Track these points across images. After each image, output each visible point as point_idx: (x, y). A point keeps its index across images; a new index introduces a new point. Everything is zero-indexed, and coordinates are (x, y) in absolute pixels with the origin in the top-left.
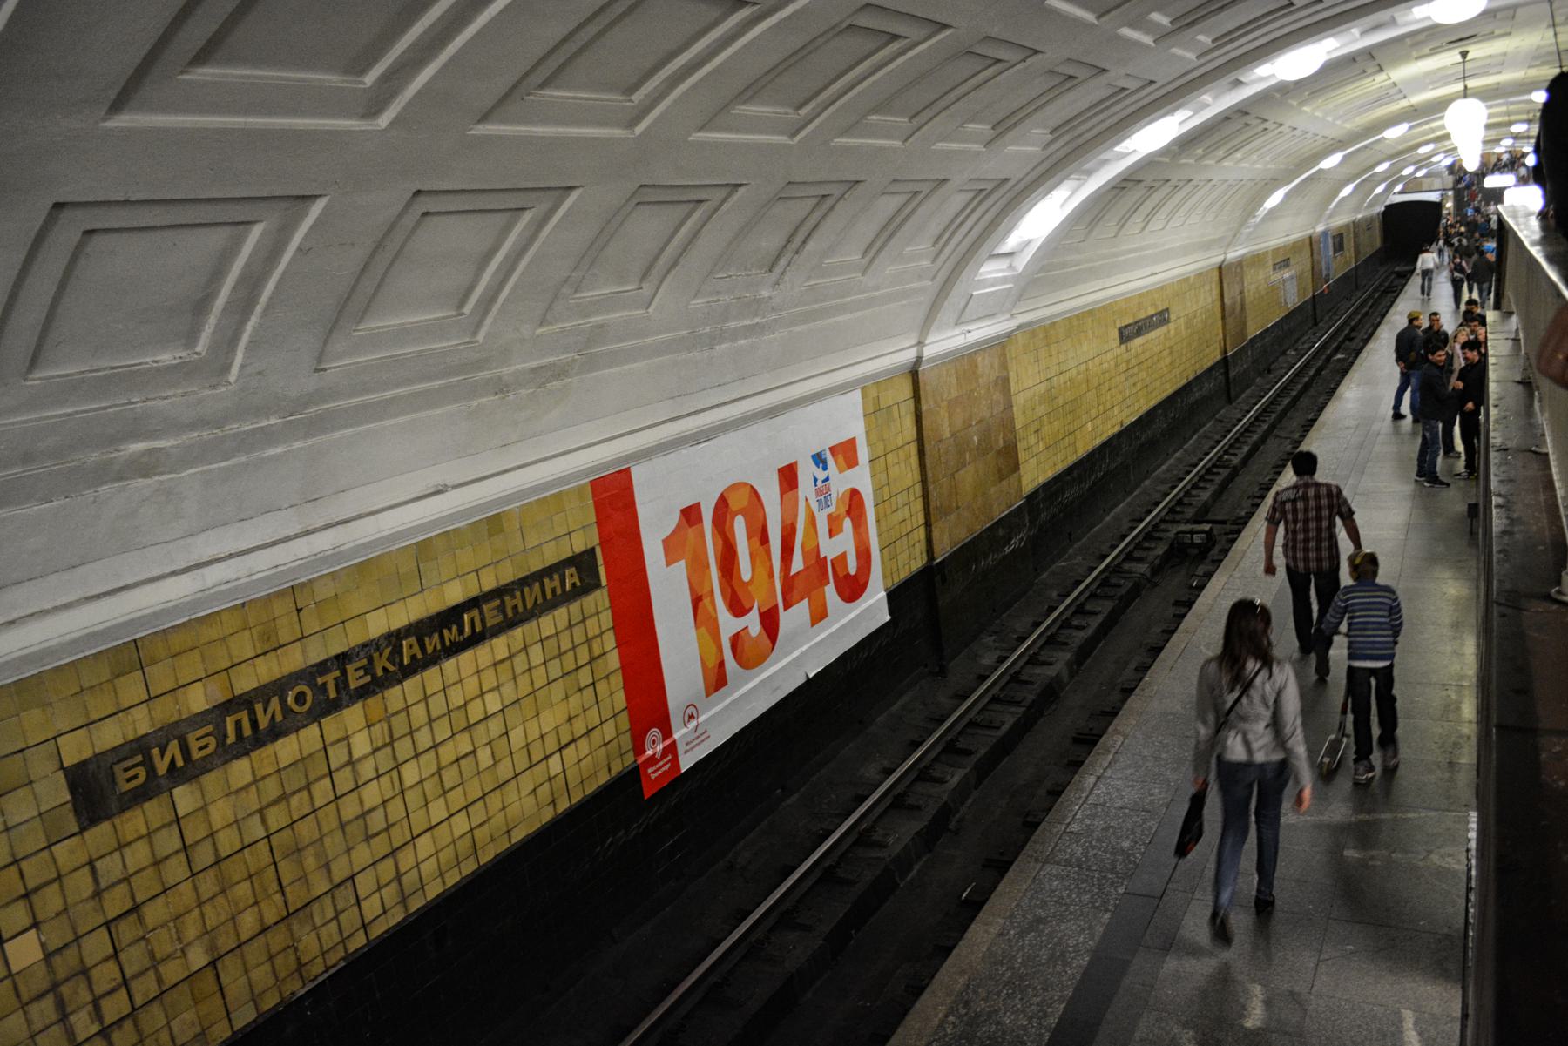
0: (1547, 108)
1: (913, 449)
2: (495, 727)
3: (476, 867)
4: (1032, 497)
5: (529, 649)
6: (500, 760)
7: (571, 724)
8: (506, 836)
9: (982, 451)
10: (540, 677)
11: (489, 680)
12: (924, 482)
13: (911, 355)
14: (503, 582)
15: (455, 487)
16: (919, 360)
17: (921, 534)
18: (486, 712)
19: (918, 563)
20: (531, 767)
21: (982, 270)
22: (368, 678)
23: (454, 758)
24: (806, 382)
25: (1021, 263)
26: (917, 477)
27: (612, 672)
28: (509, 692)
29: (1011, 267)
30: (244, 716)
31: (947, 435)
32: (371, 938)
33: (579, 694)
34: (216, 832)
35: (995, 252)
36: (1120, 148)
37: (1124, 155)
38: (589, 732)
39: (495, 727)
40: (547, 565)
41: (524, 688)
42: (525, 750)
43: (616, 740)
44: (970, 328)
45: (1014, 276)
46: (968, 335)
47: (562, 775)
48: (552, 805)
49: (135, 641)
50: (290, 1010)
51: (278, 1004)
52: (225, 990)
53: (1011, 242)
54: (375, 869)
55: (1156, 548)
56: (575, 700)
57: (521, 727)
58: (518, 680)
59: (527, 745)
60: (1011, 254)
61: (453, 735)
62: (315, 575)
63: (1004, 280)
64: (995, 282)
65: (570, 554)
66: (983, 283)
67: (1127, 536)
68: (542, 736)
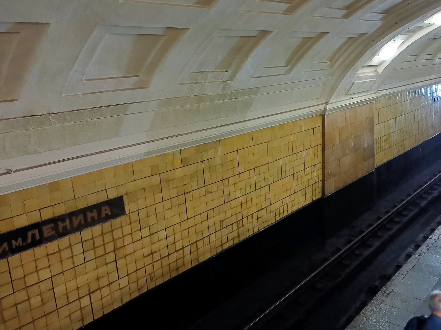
0: (404, 329)
1: (320, 148)
2: (45, 286)
3: (121, 305)
4: (378, 168)
5: (73, 247)
6: (46, 303)
7: (99, 281)
8: (102, 309)
9: (355, 149)
10: (79, 260)
11: (43, 263)
12: (323, 162)
13: (322, 107)
14: (57, 215)
15: (15, 171)
16: (325, 110)
17: (320, 184)
18: (39, 280)
19: (317, 196)
20: (68, 304)
21: (360, 71)
22: (54, 232)
23: (14, 304)
24: (225, 127)
25: (380, 70)
26: (320, 159)
27: (128, 255)
28: (56, 269)
29: (376, 71)
30: (36, 232)
31: (337, 141)
32: (148, 290)
33: (106, 266)
34: (36, 272)
35: (366, 65)
36: (427, 21)
37: (430, 25)
38: (110, 284)
39: (45, 286)
40: (78, 209)
41: (68, 264)
42: (66, 296)
43: (215, 241)
44: (353, 97)
45: (376, 75)
46: (352, 99)
47: (90, 306)
48: (81, 321)
49: (180, 150)
50: (150, 293)
51: (233, 245)
52: (93, 304)
53: (375, 61)
54: (46, 317)
55: (434, 193)
56: (102, 270)
57: (64, 285)
58: (63, 262)
59: (67, 293)
60: (376, 66)
61: (14, 292)
62: (268, 127)
63: (372, 77)
64: (366, 78)
65: (106, 199)
66: (360, 78)
67: (422, 186)
68: (78, 288)
